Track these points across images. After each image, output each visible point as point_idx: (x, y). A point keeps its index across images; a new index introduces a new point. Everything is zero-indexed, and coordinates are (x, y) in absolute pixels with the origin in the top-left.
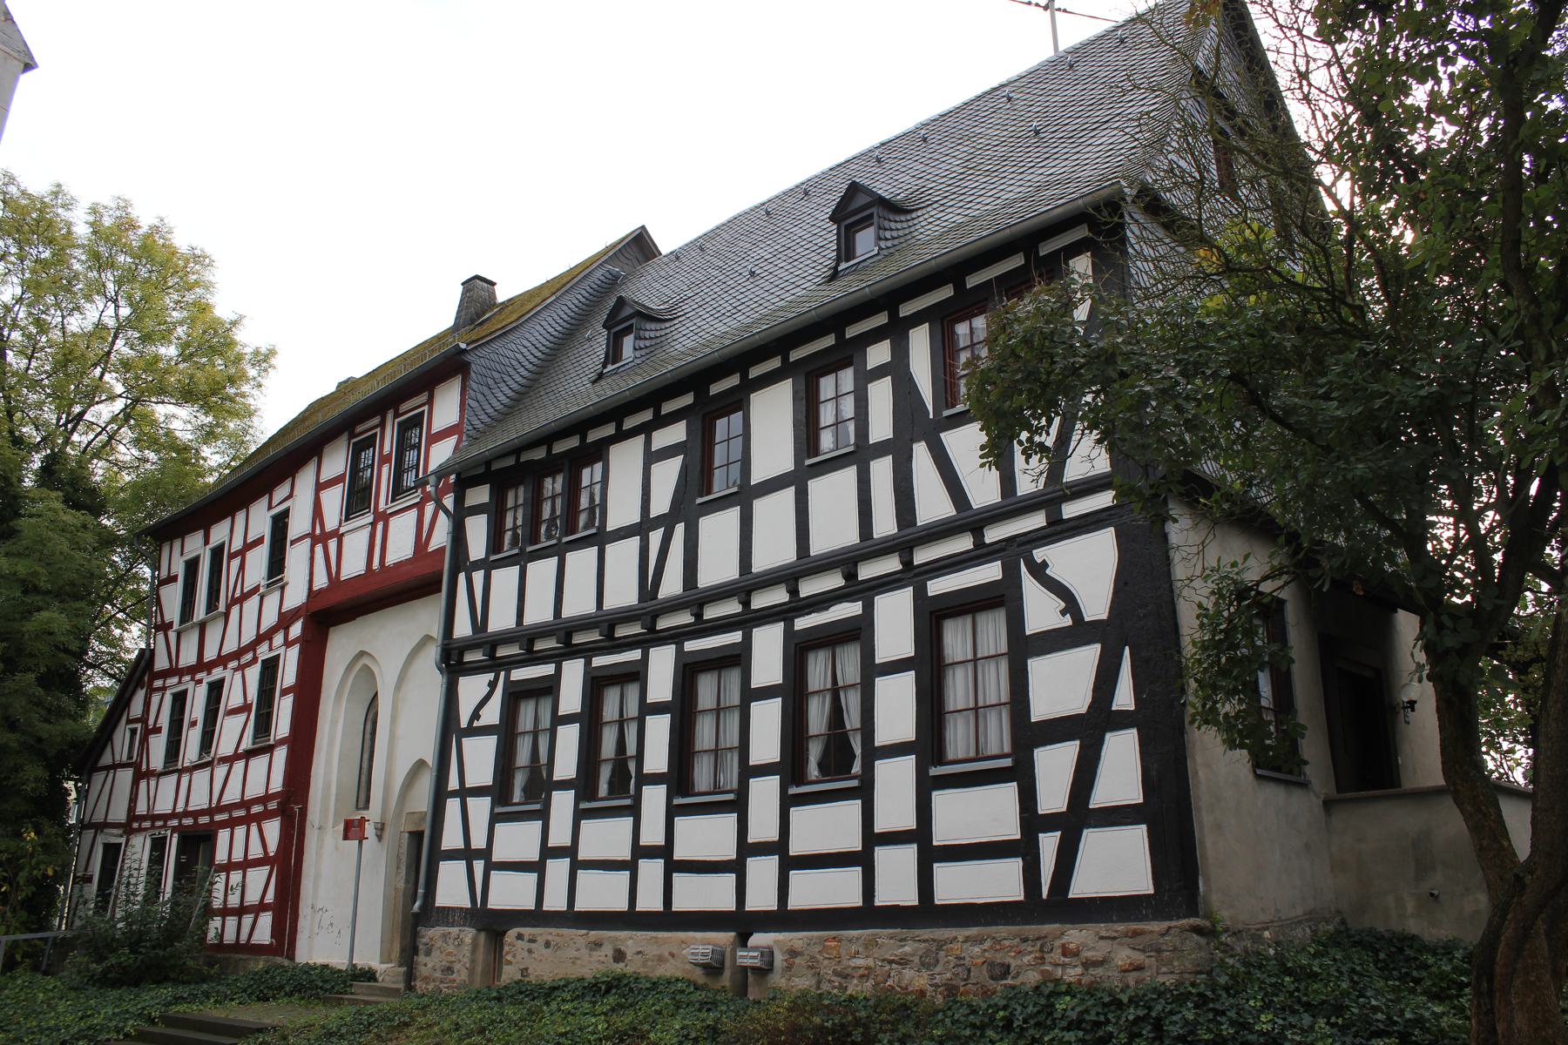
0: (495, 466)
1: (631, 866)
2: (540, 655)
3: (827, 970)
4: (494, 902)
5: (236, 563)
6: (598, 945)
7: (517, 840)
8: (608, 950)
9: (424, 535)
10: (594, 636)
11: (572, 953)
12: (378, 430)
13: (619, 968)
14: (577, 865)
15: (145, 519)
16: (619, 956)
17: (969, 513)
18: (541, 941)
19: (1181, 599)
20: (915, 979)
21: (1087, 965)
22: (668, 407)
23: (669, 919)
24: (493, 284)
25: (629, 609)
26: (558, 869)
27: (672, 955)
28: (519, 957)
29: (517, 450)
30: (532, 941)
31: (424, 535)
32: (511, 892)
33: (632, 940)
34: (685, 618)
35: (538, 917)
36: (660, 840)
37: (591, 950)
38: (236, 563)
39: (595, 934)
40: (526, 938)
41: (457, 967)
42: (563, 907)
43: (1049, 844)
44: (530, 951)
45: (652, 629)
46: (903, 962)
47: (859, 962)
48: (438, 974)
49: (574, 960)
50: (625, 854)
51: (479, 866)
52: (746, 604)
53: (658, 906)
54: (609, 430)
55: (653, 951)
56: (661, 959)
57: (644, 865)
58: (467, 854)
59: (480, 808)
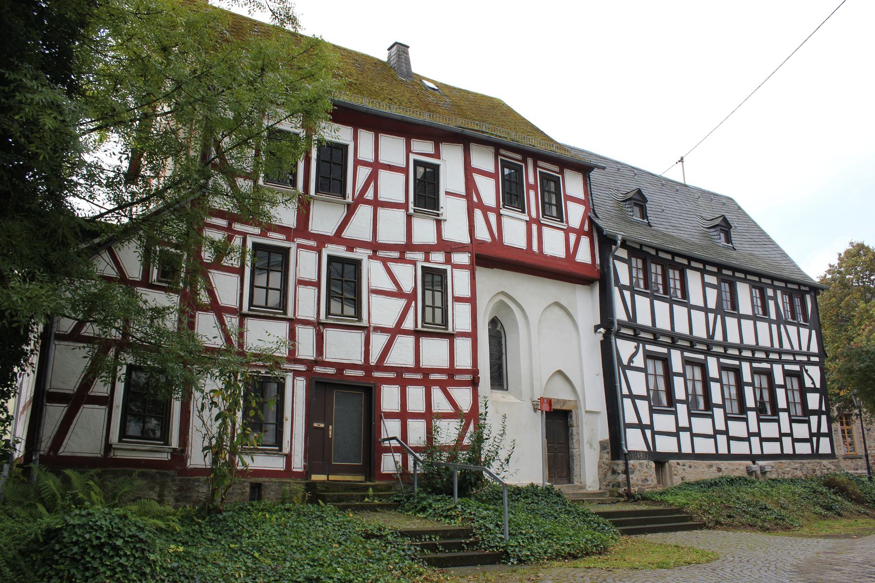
1: (714, 437)
3: (780, 471)
4: (659, 449)
6: (711, 466)
8: (715, 468)
11: (701, 470)
12: (538, 169)
13: (720, 474)
14: (693, 435)
16: (719, 470)
18: (687, 465)
20: (799, 473)
21: (828, 469)
23: (730, 457)
24: (408, 47)
25: (720, 342)
26: (685, 436)
28: (680, 472)
29: (658, 250)
30: (684, 465)
32: (666, 445)
33: (723, 464)
34: (721, 350)
35: (680, 455)
36: (756, 431)
41: (649, 479)
42: (791, 452)
43: (814, 439)
44: (684, 470)
45: (709, 349)
46: (796, 469)
47: (788, 469)
48: (640, 482)
49: (703, 472)
51: (648, 433)
52: (740, 353)
53: (726, 452)
55: (730, 468)
56: (733, 470)
57: (784, 439)
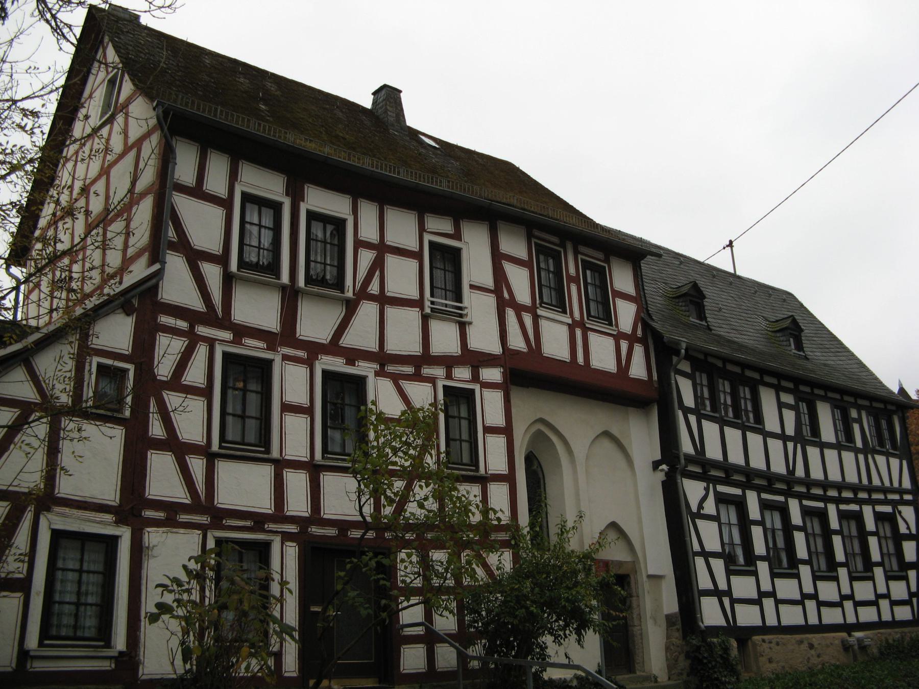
0: (710, 360)
2: (733, 481)
5: (140, 186)
7: (743, 586)
9: (624, 362)
10: (721, 474)
14: (778, 602)
15: (213, 83)
17: (703, 458)
19: (42, 437)
22: (830, 395)
27: (831, 644)
30: (770, 642)
31: (624, 362)
32: (747, 616)
35: (764, 629)
37: (799, 644)
38: (140, 186)
39: (798, 637)
40: (767, 641)
42: (776, 624)
44: (770, 648)
50: (872, 597)
51: (726, 601)
54: (822, 393)
58: (716, 592)
59: (718, 565)
